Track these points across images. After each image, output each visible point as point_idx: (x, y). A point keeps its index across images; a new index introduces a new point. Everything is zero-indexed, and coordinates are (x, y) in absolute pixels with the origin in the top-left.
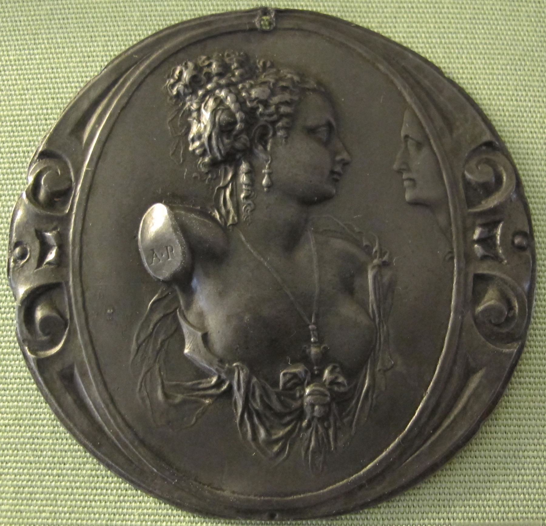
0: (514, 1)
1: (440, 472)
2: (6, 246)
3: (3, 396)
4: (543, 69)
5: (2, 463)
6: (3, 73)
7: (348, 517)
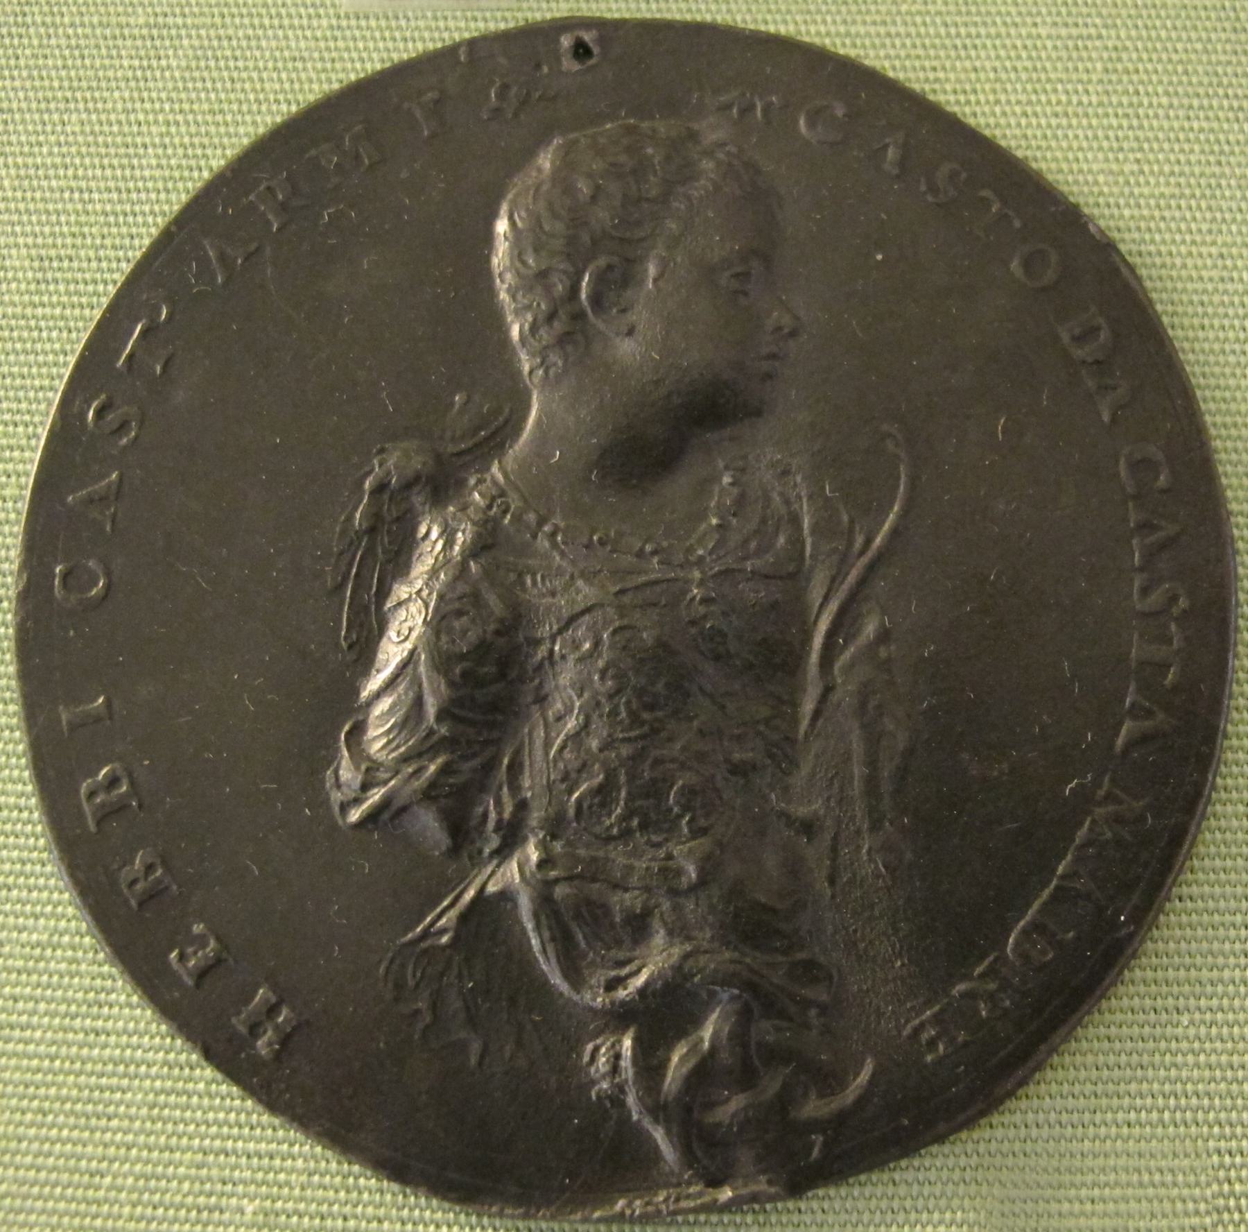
2: (11, 563)
4: (1241, 137)
6: (7, 41)
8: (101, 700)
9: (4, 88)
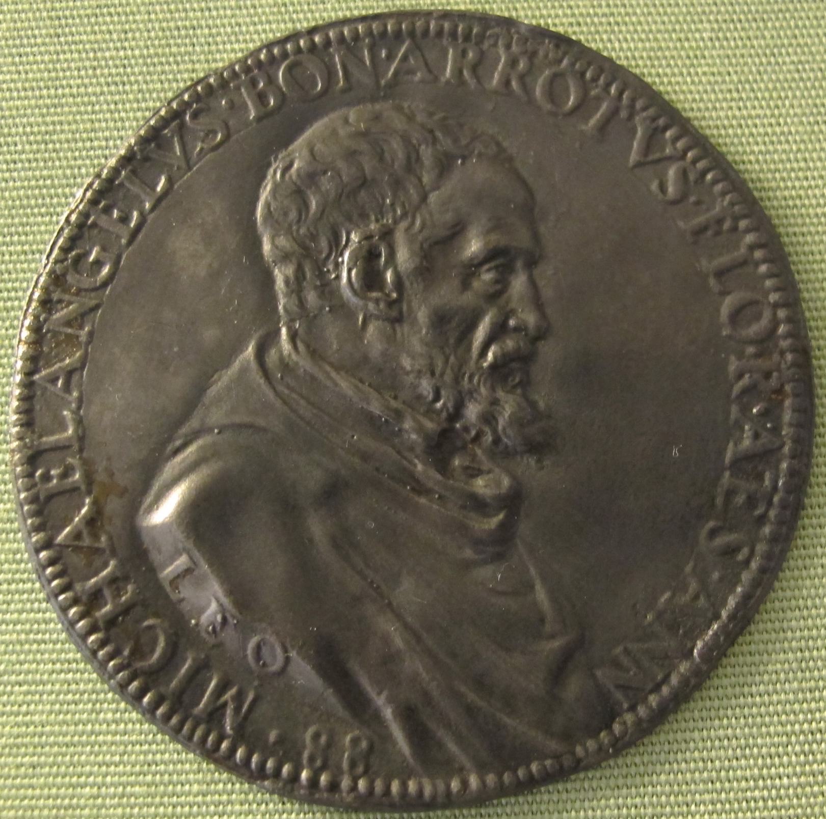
0: (792, 2)
1: (667, 727)
3: (7, 799)
5: (4, 705)
7: (551, 788)
8: (755, 411)
9: (3, 198)
